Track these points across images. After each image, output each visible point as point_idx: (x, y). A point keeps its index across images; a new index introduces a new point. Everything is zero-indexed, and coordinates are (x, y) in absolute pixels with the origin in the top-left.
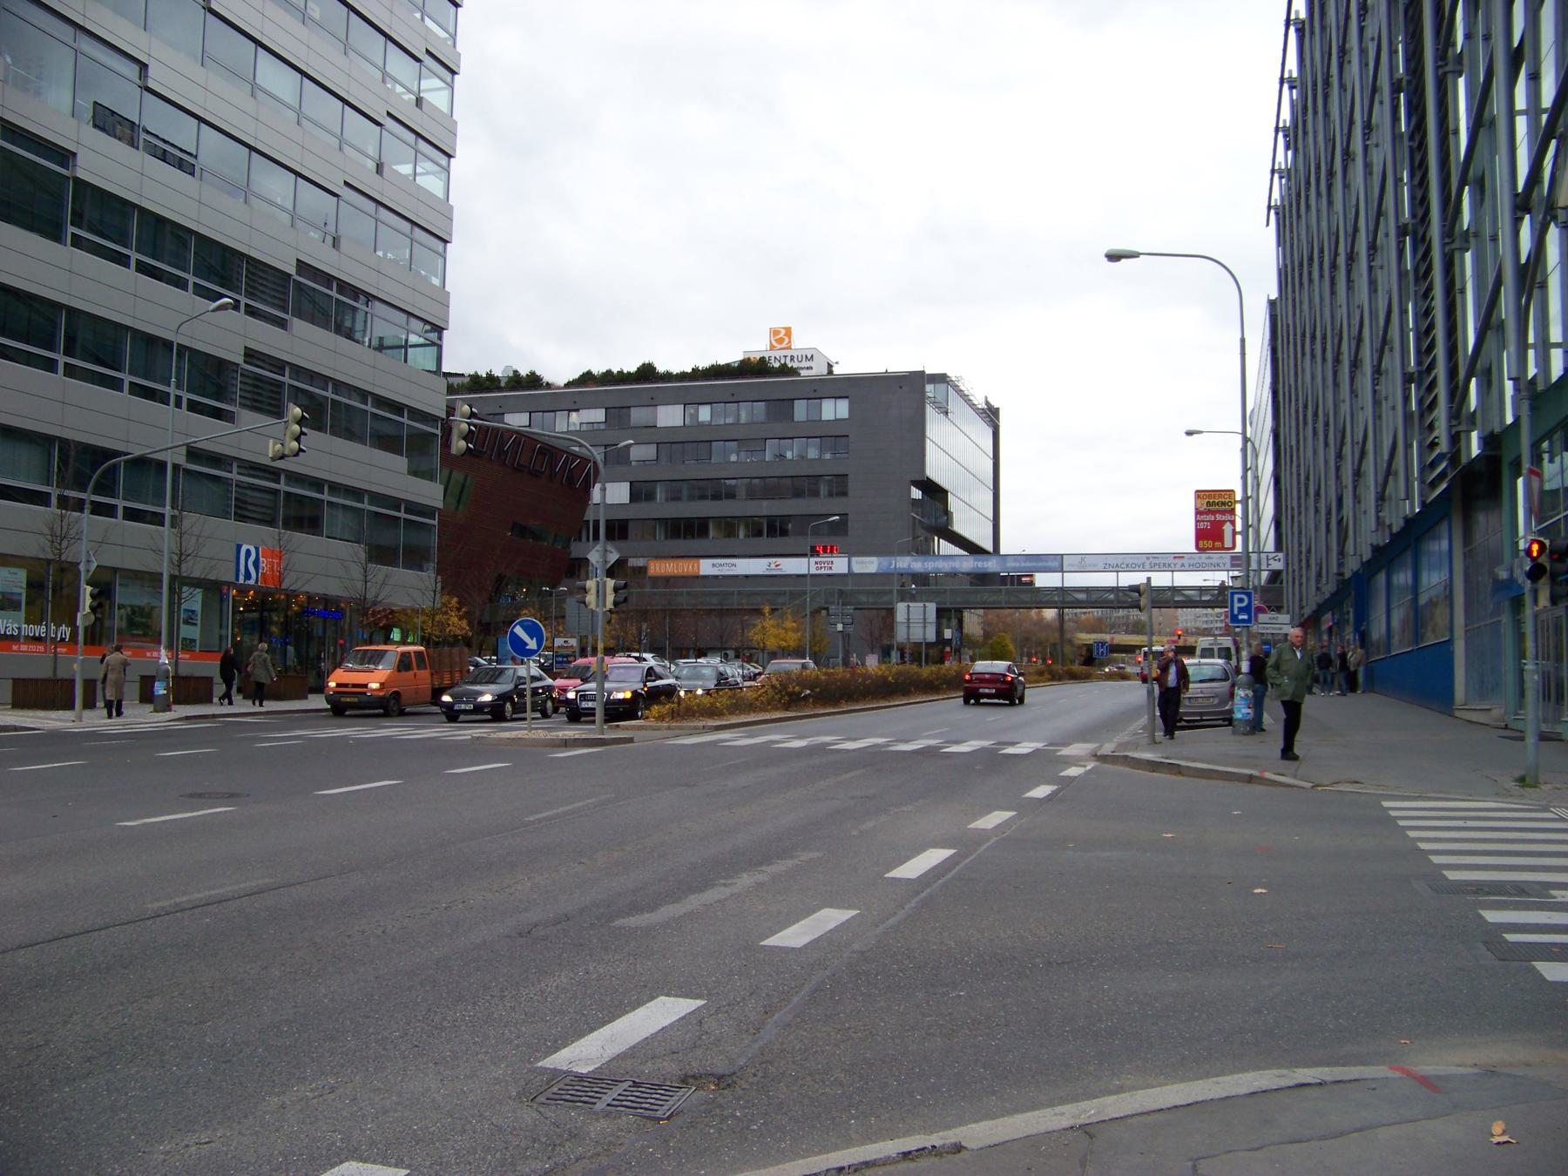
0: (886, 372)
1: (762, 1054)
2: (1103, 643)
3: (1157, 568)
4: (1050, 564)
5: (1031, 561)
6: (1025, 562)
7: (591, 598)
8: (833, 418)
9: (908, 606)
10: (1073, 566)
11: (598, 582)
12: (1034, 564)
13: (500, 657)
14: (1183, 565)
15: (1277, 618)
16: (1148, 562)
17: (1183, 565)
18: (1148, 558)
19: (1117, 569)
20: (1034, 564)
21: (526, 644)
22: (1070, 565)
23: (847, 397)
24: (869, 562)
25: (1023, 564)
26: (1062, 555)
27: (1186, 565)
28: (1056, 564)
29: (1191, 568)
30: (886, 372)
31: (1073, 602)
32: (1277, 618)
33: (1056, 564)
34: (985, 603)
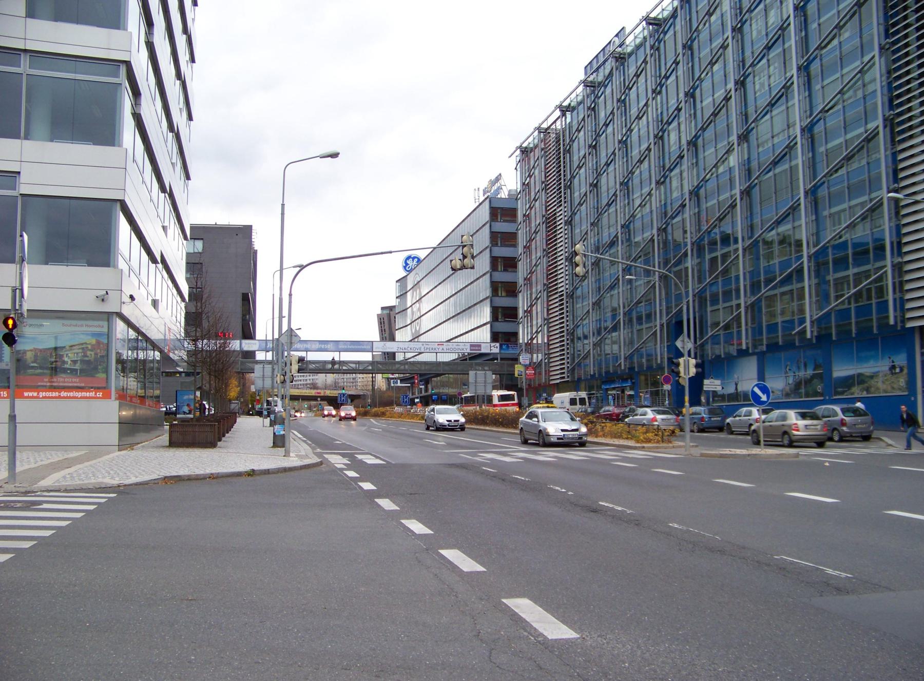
0: (216, 224)
1: (171, 676)
2: (344, 395)
3: (428, 351)
4: (365, 347)
5: (354, 345)
6: (350, 345)
7: (681, 369)
8: (193, 252)
9: (476, 374)
10: (379, 348)
11: (684, 360)
12: (357, 347)
13: (178, 404)
14: (443, 349)
15: (714, 382)
16: (423, 347)
17: (443, 349)
18: (423, 345)
19: (405, 351)
20: (357, 347)
21: (761, 398)
22: (376, 348)
23: (202, 239)
24: (253, 344)
25: (349, 347)
26: (372, 342)
27: (445, 349)
28: (369, 347)
29: (448, 351)
30: (216, 224)
31: (349, 370)
32: (714, 382)
33: (369, 347)
34: (392, 370)
